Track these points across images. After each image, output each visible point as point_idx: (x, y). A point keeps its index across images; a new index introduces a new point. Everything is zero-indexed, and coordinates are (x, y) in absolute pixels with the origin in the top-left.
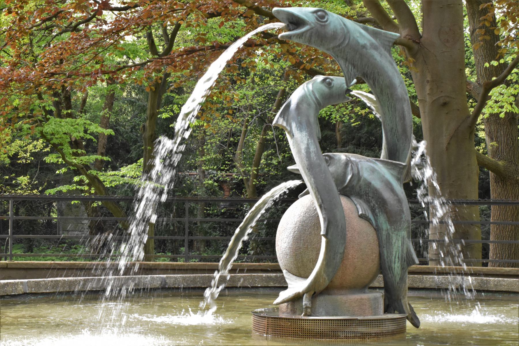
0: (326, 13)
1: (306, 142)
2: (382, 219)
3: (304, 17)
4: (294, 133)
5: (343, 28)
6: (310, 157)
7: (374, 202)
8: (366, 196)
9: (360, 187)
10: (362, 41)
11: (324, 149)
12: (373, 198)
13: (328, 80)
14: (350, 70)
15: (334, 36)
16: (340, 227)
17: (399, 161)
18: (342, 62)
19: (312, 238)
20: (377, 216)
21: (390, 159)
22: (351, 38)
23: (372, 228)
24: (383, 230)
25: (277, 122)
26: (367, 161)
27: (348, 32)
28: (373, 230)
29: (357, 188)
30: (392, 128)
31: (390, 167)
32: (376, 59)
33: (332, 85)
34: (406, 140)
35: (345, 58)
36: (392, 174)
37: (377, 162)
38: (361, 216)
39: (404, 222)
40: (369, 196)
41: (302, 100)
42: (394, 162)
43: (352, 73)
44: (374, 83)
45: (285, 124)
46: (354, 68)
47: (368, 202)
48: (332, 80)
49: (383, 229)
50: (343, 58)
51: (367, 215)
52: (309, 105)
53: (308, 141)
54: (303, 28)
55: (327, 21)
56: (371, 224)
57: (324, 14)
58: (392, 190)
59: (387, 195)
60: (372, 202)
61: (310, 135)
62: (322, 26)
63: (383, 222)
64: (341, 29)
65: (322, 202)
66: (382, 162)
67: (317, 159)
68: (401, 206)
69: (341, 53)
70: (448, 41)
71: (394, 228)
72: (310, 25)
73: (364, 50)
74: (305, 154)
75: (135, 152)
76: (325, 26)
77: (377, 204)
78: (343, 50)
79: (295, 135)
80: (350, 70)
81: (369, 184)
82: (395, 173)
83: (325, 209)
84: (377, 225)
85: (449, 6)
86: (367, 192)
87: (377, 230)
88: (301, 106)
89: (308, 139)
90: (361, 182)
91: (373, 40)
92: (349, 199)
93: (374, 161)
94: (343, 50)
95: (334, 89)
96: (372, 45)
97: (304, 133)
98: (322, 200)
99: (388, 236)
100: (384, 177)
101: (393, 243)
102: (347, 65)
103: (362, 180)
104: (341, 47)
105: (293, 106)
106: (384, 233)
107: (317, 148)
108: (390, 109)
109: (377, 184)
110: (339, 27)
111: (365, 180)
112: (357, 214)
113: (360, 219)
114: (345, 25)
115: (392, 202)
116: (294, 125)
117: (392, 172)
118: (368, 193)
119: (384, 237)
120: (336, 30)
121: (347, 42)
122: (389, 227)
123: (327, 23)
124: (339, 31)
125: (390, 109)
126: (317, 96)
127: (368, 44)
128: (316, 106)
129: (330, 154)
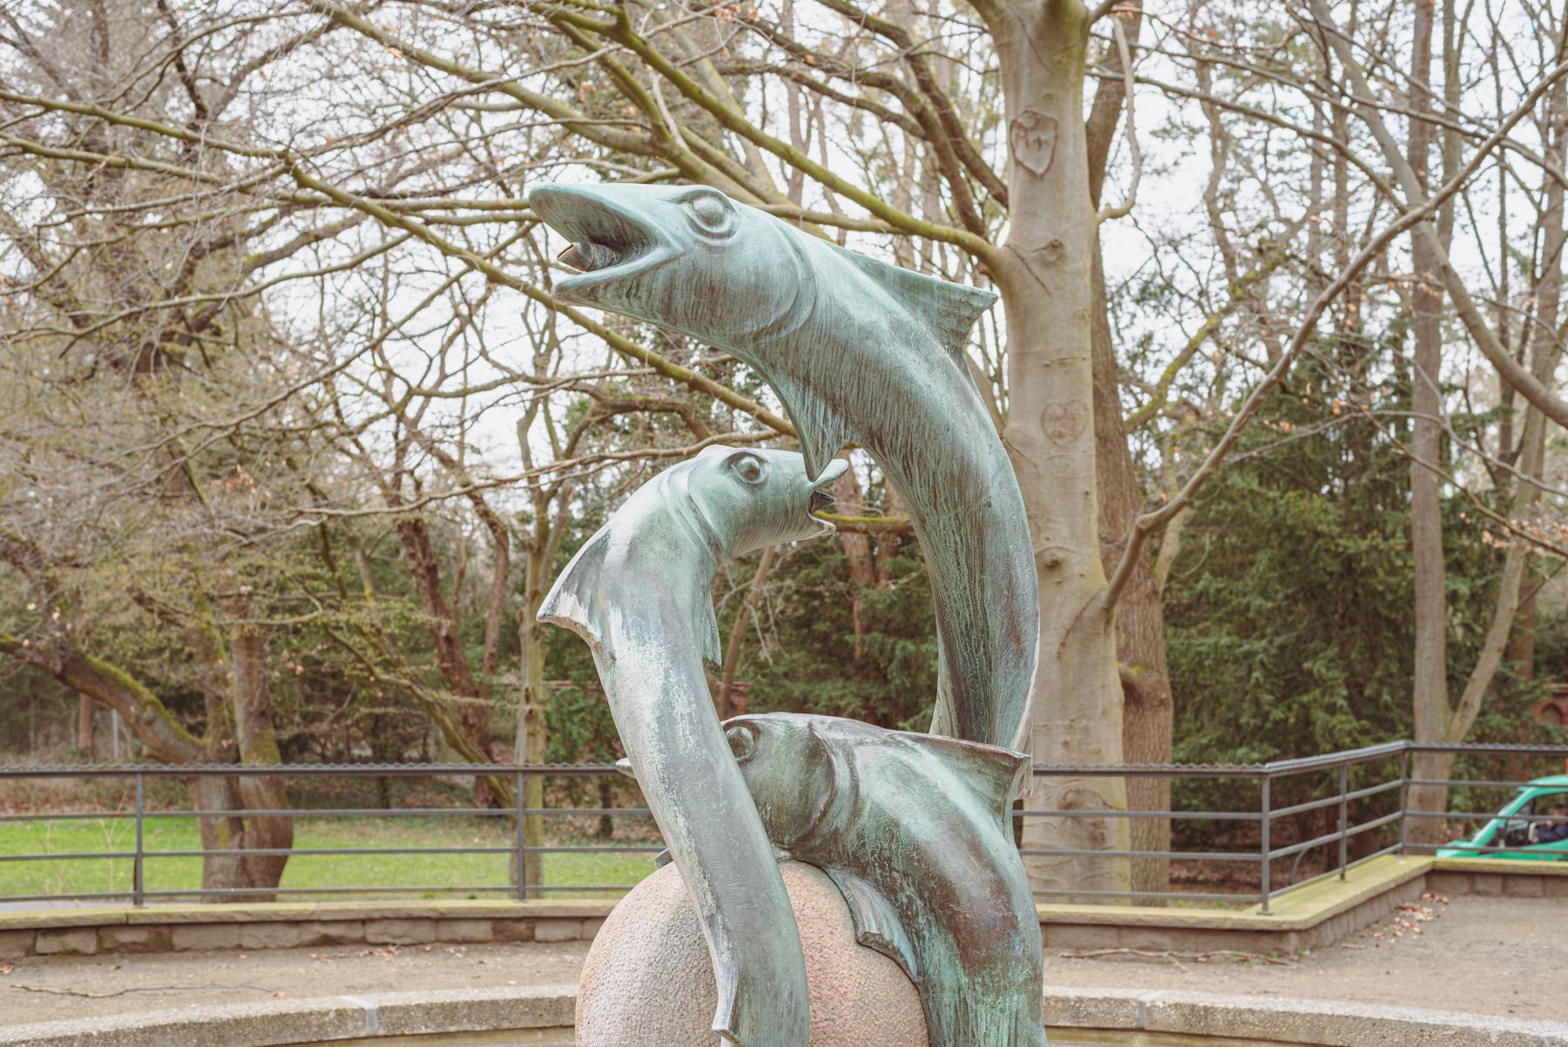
0: (728, 206)
1: (658, 681)
2: (940, 954)
3: (646, 218)
4: (616, 647)
5: (791, 261)
6: (674, 736)
7: (910, 891)
8: (882, 867)
9: (860, 836)
10: (862, 314)
11: (727, 707)
12: (906, 875)
13: (746, 460)
14: (820, 419)
15: (758, 294)
16: (786, 995)
17: (989, 742)
18: (792, 389)
19: (689, 1026)
20: (921, 937)
21: (963, 737)
22: (821, 304)
23: (906, 982)
24: (943, 990)
25: (553, 607)
26: (885, 743)
27: (811, 276)
28: (909, 986)
29: (851, 840)
30: (969, 627)
31: (965, 766)
32: (912, 381)
33: (762, 478)
34: (1016, 666)
35: (801, 373)
36: (973, 790)
37: (918, 747)
38: (865, 942)
39: (1018, 960)
40: (892, 869)
41: (653, 527)
42: (979, 746)
43: (830, 433)
44: (907, 468)
45: (581, 617)
46: (834, 412)
47: (889, 891)
48: (761, 461)
49: (942, 985)
50: (792, 374)
51: (887, 937)
52: (674, 545)
53: (666, 677)
54: (641, 256)
55: (729, 234)
56: (902, 967)
57: (720, 208)
58: (976, 849)
59: (955, 865)
60: (902, 889)
61: (676, 657)
62: (710, 248)
63: (944, 962)
64: (782, 265)
65: (718, 907)
66: (935, 745)
67: (698, 744)
68: (1008, 905)
69: (784, 355)
70: (1061, 435)
71: (984, 984)
72: (668, 244)
73: (870, 343)
74: (654, 725)
75: (999, 608)
76: (721, 249)
77: (921, 897)
78: (792, 345)
79: (617, 655)
80: (820, 419)
81: (891, 828)
82: (985, 787)
83: (727, 931)
84: (922, 972)
85: (1062, 362)
86: (887, 854)
87: (923, 986)
88: (643, 549)
89: (666, 671)
90: (865, 820)
91: (904, 314)
92: (824, 878)
93: (909, 743)
94: (792, 345)
95: (767, 491)
96: (898, 327)
97: (654, 649)
98: (717, 899)
99: (962, 1008)
100: (945, 798)
101: (980, 1037)
102: (808, 402)
103: (866, 813)
104: (784, 333)
105: (616, 552)
106: (948, 999)
107: (698, 698)
108: (963, 560)
109: (920, 826)
110: (775, 259)
111: (878, 811)
112: (850, 933)
113: (863, 951)
114: (798, 251)
115: (975, 892)
116: (615, 619)
117: (973, 781)
118: (889, 860)
119: (948, 1014)
120: (767, 268)
121: (805, 314)
122: (964, 980)
123: (728, 242)
124: (777, 273)
125: (963, 560)
126: (708, 516)
127: (885, 325)
128: (703, 552)
129: (756, 718)
